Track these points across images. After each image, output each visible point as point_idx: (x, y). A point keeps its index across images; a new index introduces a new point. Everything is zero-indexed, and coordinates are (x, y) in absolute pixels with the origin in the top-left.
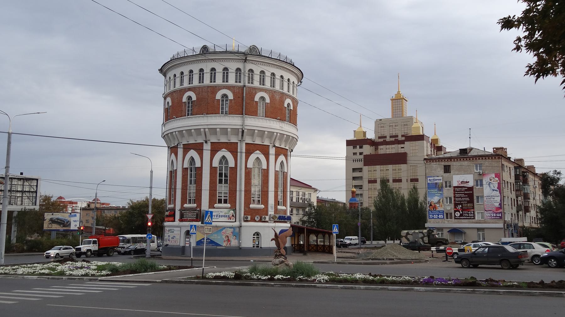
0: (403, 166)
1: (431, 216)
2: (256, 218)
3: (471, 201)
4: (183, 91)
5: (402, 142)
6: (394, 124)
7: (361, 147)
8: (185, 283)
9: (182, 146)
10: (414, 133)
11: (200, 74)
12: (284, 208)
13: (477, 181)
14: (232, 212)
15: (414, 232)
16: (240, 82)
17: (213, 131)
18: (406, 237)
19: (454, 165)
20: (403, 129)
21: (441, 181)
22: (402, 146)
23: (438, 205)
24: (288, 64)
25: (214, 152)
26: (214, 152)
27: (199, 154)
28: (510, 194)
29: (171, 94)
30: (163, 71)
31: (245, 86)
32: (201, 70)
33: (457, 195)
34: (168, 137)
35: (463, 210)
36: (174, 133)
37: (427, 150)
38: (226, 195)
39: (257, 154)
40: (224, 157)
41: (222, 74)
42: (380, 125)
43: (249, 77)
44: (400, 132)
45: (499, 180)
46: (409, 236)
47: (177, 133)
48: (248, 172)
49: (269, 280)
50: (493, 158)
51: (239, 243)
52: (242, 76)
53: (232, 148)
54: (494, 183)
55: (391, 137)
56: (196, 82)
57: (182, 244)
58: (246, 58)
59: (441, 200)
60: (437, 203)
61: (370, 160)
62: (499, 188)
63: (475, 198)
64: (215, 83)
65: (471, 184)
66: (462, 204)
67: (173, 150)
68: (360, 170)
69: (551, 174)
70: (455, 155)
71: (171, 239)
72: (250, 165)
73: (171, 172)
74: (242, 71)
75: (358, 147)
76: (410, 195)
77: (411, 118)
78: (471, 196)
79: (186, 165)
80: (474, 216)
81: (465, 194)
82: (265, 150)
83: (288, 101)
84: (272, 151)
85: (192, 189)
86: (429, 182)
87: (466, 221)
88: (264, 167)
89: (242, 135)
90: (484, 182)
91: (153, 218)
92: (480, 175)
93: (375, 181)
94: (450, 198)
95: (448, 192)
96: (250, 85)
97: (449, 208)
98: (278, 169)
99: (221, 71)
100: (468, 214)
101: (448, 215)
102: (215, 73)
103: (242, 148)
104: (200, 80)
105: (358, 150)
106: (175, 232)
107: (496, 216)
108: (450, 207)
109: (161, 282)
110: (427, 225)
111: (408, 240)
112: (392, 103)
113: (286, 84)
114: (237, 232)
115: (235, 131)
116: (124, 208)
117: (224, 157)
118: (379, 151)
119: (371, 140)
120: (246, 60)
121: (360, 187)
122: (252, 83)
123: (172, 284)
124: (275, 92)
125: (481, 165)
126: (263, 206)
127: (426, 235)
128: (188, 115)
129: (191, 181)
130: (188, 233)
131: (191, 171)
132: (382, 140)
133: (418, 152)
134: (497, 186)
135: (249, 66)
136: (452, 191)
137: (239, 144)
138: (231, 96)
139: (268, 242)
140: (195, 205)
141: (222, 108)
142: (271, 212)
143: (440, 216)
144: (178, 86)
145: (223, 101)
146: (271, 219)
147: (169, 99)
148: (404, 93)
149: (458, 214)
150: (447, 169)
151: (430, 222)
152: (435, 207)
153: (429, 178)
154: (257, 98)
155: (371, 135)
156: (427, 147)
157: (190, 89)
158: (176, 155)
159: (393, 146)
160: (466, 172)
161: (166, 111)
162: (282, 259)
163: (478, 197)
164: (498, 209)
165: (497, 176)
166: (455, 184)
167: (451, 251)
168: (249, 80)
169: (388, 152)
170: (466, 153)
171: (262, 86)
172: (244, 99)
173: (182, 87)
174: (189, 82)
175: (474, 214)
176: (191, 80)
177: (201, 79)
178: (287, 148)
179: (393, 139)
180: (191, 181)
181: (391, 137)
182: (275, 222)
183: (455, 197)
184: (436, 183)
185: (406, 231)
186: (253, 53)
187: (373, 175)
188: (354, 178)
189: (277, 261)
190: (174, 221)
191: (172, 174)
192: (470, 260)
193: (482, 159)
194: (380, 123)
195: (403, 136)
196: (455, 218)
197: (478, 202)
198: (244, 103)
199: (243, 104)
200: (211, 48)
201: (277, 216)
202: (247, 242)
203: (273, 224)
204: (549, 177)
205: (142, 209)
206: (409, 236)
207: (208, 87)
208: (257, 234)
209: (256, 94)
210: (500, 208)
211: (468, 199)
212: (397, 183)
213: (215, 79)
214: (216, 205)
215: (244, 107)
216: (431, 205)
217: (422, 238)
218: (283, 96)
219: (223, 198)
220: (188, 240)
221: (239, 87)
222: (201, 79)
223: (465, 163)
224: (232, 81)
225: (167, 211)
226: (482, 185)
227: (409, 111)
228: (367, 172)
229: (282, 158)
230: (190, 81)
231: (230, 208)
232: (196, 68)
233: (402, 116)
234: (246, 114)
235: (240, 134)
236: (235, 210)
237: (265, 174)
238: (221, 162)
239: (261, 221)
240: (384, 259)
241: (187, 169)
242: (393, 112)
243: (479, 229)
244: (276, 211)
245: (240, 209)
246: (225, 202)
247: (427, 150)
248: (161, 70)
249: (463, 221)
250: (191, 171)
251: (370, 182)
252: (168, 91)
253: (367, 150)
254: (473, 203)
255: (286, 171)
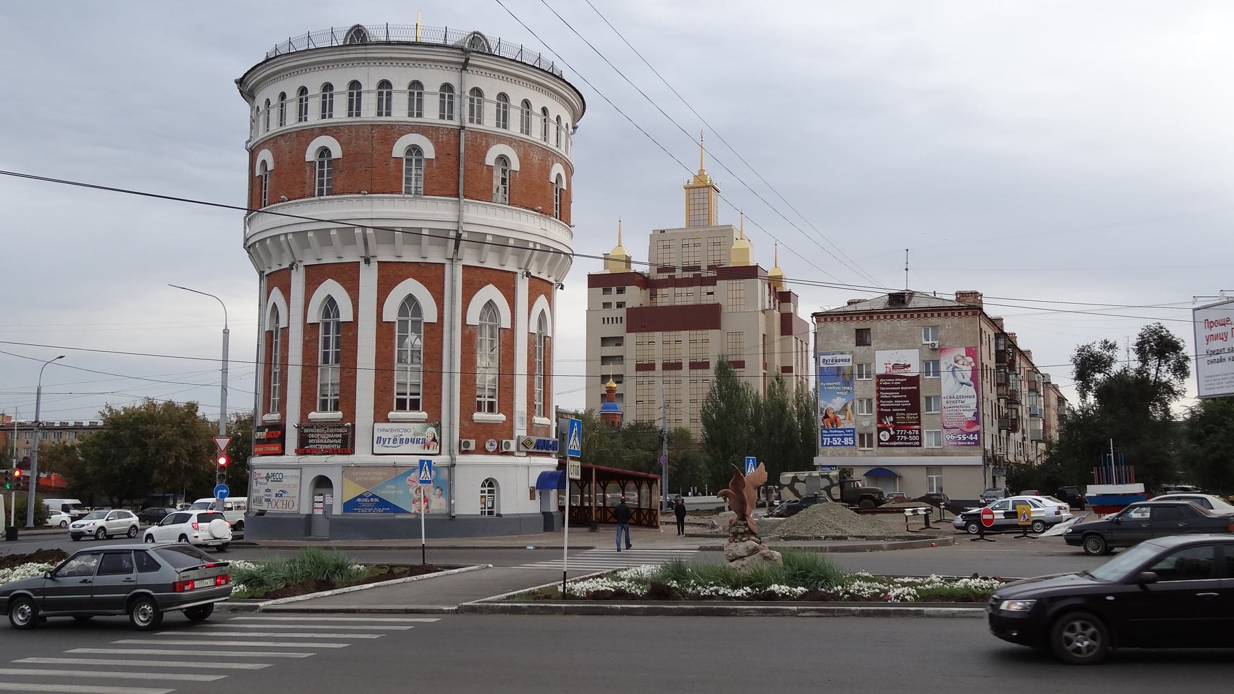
0: (712, 334)
1: (827, 440)
2: (487, 446)
3: (915, 407)
4: (310, 134)
5: (712, 281)
6: (691, 242)
7: (620, 291)
8: (504, 611)
9: (302, 270)
10: (734, 262)
11: (351, 95)
12: (545, 421)
13: (927, 365)
14: (433, 430)
15: (810, 476)
16: (450, 118)
17: (387, 233)
18: (791, 487)
19: (879, 327)
20: (711, 253)
21: (850, 364)
22: (710, 289)
23: (842, 417)
24: (549, 78)
25: (387, 283)
26: (387, 283)
27: (348, 290)
28: (990, 393)
29: (271, 142)
30: (247, 86)
31: (463, 128)
32: (355, 85)
33: (884, 395)
34: (256, 250)
35: (896, 426)
36: (282, 238)
37: (763, 300)
38: (415, 391)
39: (490, 292)
40: (410, 298)
41: (406, 96)
42: (660, 244)
43: (472, 107)
44: (703, 259)
45: (975, 362)
46: (797, 486)
47: (290, 237)
48: (469, 337)
49: (751, 599)
50: (949, 313)
51: (450, 505)
52: (456, 101)
53: (432, 276)
54: (964, 368)
55: (685, 269)
56: (340, 114)
57: (305, 510)
58: (467, 59)
59: (849, 406)
60: (839, 412)
61: (640, 320)
62: (974, 378)
63: (923, 401)
64: (388, 118)
65: (914, 370)
66: (893, 414)
67: (276, 280)
68: (618, 341)
69: (1097, 349)
70: (880, 306)
71: (273, 497)
72: (473, 318)
73: (270, 334)
74: (457, 92)
75: (614, 289)
76: (770, 392)
77: (728, 229)
78: (914, 397)
79: (314, 316)
80: (920, 441)
81: (901, 392)
82: (506, 283)
83: (557, 169)
84: (522, 288)
85: (329, 376)
86: (822, 365)
87: (903, 450)
88: (506, 323)
89: (457, 247)
90: (943, 367)
91: (229, 445)
92: (934, 350)
93: (705, 365)
94: (869, 400)
95: (865, 388)
96: (475, 125)
97: (866, 423)
98: (534, 329)
99: (405, 88)
100: (908, 435)
101: (865, 439)
102: (389, 94)
103: (454, 280)
104: (350, 108)
105: (614, 297)
106: (284, 482)
107: (968, 440)
108: (867, 420)
109: (456, 612)
110: (817, 461)
111: (796, 493)
112: (688, 195)
113: (552, 128)
114: (445, 482)
115: (439, 236)
116: (93, 427)
117: (410, 298)
118: (659, 300)
119: (641, 274)
120: (465, 66)
121: (619, 379)
122: (479, 122)
123: (567, 618)
124: (530, 145)
125: (935, 328)
126: (501, 417)
127: (836, 482)
128: (321, 193)
129: (326, 355)
130: (323, 483)
131: (327, 331)
132: (665, 276)
133: (745, 306)
134: (969, 374)
135: (473, 80)
136: (874, 386)
137: (447, 268)
138: (429, 151)
139: (517, 499)
140: (339, 414)
141: (408, 180)
142: (521, 431)
143: (846, 441)
144: (292, 122)
145: (409, 161)
146: (522, 448)
147: (266, 155)
148: (715, 176)
149: (885, 436)
150: (862, 338)
151: (824, 454)
152: (835, 421)
153: (822, 358)
154: (490, 159)
155: (641, 266)
156: (763, 292)
157: (324, 131)
158: (286, 292)
159: (690, 289)
160: (903, 343)
161: (256, 184)
162: (751, 543)
163: (928, 399)
164: (971, 423)
165: (970, 352)
166: (880, 369)
167: (990, 517)
168: (472, 113)
169: (679, 302)
170: (903, 302)
171: (501, 130)
172: (462, 159)
173: (303, 124)
174: (323, 113)
175: (920, 435)
176: (327, 109)
177: (354, 106)
178: (552, 280)
179: (690, 275)
180: (326, 355)
181: (685, 269)
182: (529, 454)
183: (879, 399)
184: (839, 368)
185: (791, 475)
186: (472, 52)
187: (700, 351)
188: (605, 360)
189: (740, 548)
190: (283, 454)
191: (273, 342)
192: (1108, 536)
193: (939, 315)
194: (660, 239)
195: (710, 268)
196: (879, 446)
197: (929, 408)
198: (462, 169)
199: (458, 168)
200: (376, 33)
201: (534, 439)
202: (468, 503)
203: (526, 460)
204: (1092, 355)
205: (142, 427)
206: (797, 486)
207: (373, 126)
208: (490, 483)
209: (488, 147)
210: (977, 422)
211: (907, 403)
212: (700, 371)
213: (359, 108)
214: (391, 415)
215: (461, 179)
216: (826, 416)
217: (828, 489)
218: (549, 156)
219: (408, 397)
220: (320, 498)
221: (450, 130)
222: (354, 106)
223: (902, 325)
224: (431, 114)
225: (260, 429)
226: (937, 372)
227: (723, 216)
228: (634, 346)
229: (542, 302)
230: (324, 110)
231: (426, 421)
232: (340, 79)
233: (709, 225)
234: (465, 197)
235: (452, 243)
236: (438, 427)
237: (507, 339)
238: (403, 310)
239: (498, 452)
240: (818, 538)
241: (316, 325)
242: (688, 216)
243: (929, 468)
244: (531, 427)
245: (451, 424)
246: (415, 406)
247: (763, 300)
248: (241, 82)
249: (897, 450)
250: (327, 331)
251: (640, 367)
252: (262, 134)
253: (635, 297)
254: (918, 411)
255: (549, 334)
